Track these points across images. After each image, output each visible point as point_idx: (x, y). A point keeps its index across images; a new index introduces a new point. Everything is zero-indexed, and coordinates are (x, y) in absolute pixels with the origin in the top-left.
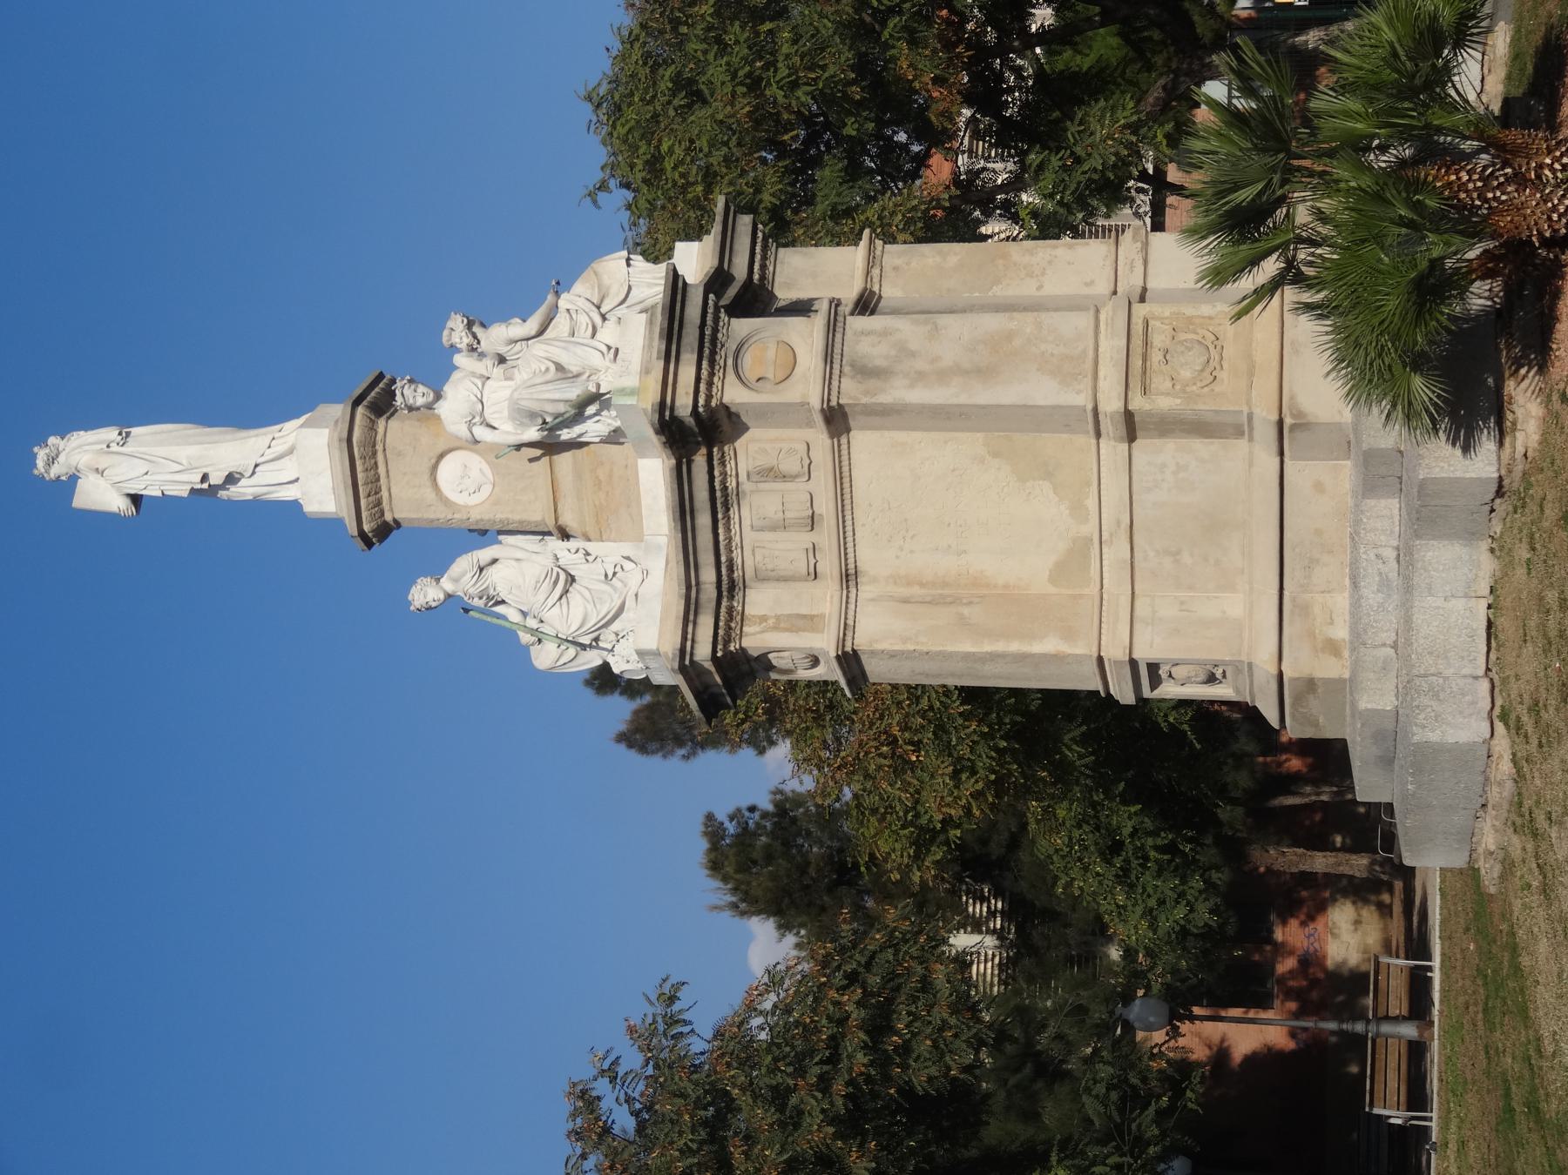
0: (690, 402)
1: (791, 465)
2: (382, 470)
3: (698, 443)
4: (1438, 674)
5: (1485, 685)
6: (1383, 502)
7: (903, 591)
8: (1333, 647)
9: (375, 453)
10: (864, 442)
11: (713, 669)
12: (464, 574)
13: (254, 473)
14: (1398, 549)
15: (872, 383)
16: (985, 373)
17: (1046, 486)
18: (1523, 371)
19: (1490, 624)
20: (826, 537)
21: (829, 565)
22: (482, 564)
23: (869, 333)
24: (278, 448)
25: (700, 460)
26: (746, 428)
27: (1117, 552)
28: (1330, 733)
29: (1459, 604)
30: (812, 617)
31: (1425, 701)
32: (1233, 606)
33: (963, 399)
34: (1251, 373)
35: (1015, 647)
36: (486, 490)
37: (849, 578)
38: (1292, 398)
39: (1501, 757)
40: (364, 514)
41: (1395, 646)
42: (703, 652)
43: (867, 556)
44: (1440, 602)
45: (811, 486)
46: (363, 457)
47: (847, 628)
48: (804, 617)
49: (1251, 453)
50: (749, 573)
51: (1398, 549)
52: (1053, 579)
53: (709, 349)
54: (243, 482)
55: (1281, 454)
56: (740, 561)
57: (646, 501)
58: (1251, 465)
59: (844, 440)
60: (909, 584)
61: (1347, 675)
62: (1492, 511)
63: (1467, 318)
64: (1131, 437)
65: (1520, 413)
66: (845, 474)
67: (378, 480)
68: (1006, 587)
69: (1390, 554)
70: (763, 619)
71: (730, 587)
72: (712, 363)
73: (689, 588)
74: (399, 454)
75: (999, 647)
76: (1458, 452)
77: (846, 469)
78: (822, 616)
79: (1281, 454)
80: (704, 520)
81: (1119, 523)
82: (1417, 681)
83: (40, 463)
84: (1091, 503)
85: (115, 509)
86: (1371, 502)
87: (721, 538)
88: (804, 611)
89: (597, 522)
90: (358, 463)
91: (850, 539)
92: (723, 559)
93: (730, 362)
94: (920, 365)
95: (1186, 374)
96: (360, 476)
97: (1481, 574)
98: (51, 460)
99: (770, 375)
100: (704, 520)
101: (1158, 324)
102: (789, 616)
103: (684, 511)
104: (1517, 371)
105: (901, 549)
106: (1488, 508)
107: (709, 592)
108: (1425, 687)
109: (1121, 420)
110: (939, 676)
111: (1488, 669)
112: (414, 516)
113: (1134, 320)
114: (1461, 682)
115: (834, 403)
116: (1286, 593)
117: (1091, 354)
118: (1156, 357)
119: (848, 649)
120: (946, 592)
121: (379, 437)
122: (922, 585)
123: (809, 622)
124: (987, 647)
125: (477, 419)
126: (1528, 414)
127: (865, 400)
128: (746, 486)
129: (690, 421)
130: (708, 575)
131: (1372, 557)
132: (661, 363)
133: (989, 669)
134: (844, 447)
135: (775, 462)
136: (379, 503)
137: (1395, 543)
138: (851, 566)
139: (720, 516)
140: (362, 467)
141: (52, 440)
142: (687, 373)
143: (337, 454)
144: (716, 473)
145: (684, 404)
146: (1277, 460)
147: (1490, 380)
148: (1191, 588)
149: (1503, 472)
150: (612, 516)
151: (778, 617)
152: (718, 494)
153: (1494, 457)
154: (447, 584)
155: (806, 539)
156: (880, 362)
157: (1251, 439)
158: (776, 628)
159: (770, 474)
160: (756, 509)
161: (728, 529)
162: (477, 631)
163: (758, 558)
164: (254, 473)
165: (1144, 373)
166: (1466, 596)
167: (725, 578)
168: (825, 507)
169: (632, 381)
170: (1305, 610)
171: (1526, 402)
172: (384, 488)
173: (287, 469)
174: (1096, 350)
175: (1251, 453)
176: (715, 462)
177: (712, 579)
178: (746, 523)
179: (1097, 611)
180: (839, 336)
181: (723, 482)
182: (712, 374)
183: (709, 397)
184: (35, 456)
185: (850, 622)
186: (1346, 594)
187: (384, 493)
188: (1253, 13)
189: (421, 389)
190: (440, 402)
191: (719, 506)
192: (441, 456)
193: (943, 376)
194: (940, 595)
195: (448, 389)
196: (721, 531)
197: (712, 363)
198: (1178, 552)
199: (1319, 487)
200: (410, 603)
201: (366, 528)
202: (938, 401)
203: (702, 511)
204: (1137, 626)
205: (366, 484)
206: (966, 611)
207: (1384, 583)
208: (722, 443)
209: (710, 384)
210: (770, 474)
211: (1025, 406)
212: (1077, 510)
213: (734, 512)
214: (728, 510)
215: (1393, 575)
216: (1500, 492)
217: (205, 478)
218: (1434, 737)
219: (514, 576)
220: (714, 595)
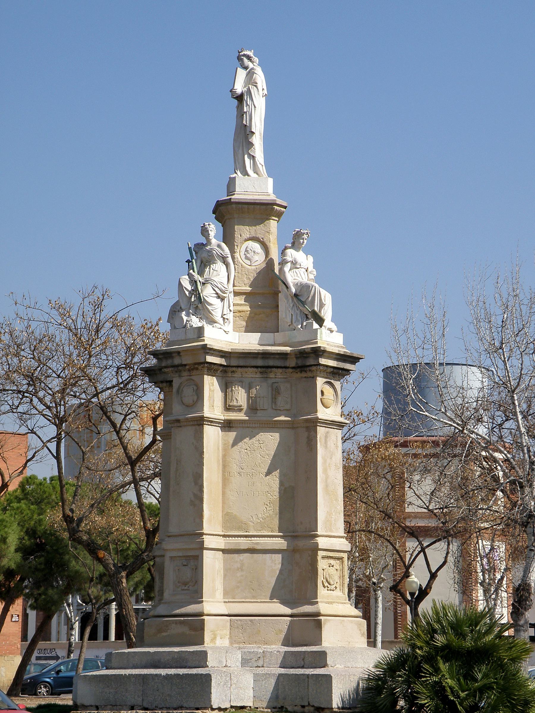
4: (231, 685)
8: (213, 640)
32: (219, 595)
41: (226, 666)
80: (260, 362)
94: (328, 461)
99: (324, 397)
106: (307, 704)
114: (229, 695)
118: (332, 562)
145: (323, 361)
156: (328, 446)
193: (325, 471)
198: (242, 570)
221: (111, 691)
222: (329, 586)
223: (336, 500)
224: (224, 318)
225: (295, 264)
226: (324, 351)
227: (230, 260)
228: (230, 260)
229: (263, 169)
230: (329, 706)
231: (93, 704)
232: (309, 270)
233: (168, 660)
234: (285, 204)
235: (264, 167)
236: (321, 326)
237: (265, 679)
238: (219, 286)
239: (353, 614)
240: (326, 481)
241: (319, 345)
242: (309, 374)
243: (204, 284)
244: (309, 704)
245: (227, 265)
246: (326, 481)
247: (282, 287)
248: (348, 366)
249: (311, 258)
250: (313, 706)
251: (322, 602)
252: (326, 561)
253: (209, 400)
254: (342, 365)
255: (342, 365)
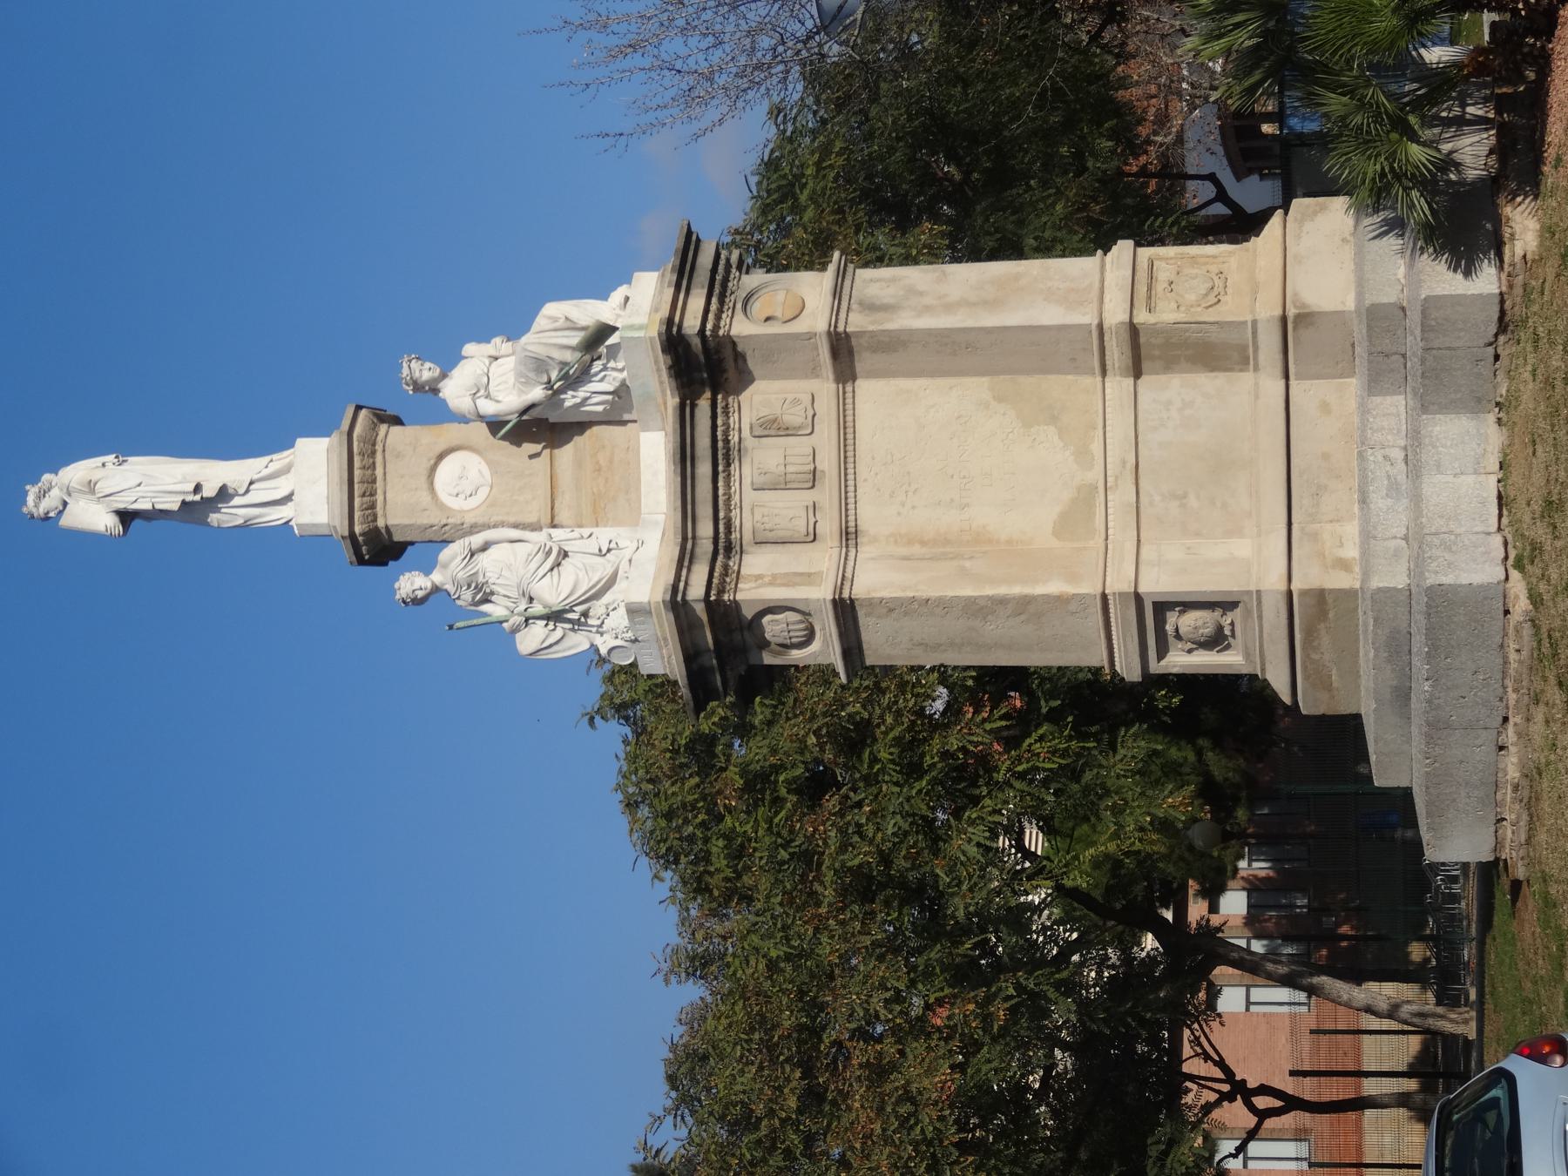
0: (698, 323)
1: (794, 417)
2: (379, 471)
3: (703, 383)
4: (1451, 532)
5: (1497, 541)
6: (1389, 399)
7: (904, 551)
8: (1343, 565)
9: (374, 453)
10: (869, 391)
11: (704, 618)
12: (454, 558)
13: (247, 491)
14: (1405, 448)
15: (879, 315)
16: (992, 304)
17: (1052, 428)
18: (1519, 199)
19: (1500, 497)
20: (826, 495)
21: (829, 526)
22: (474, 547)
23: (878, 280)
24: (273, 467)
25: (704, 404)
26: (752, 381)
27: (1122, 495)
28: (1345, 709)
29: (1470, 479)
30: (809, 575)
31: (1438, 553)
32: (1242, 548)
33: (970, 323)
34: (1255, 292)
35: (1017, 590)
36: (483, 493)
37: (849, 535)
38: (1296, 294)
39: (1517, 597)
40: (357, 515)
41: (1406, 538)
42: (696, 590)
43: (868, 515)
44: (1450, 478)
45: (813, 440)
46: (362, 454)
47: (843, 580)
48: (802, 574)
49: (1256, 384)
50: (747, 536)
51: (1405, 448)
52: (1057, 534)
53: (719, 289)
54: (237, 501)
55: (1287, 377)
56: (737, 523)
57: (645, 476)
58: (1257, 397)
59: (849, 388)
60: (910, 542)
61: (1357, 585)
62: (1497, 357)
63: (1462, 183)
64: (1137, 373)
65: (1518, 228)
66: (850, 424)
67: (374, 481)
68: (1009, 542)
69: (1398, 455)
70: (759, 577)
71: (726, 546)
72: (722, 302)
73: (685, 539)
74: (397, 456)
75: (1002, 590)
76: (1460, 276)
77: (849, 418)
78: (820, 574)
79: (1287, 377)
80: (704, 469)
81: (1124, 463)
82: (1429, 538)
83: (30, 499)
84: (1097, 447)
85: (101, 528)
86: (1378, 400)
87: (721, 492)
88: (801, 570)
89: (595, 511)
90: (357, 459)
91: (851, 494)
92: (722, 515)
93: (739, 306)
94: (927, 300)
95: (1191, 297)
96: (357, 473)
97: (1490, 449)
98: (43, 494)
99: (778, 314)
100: (704, 469)
101: (1163, 264)
102: (787, 574)
103: (684, 457)
104: (1513, 199)
105: (903, 505)
106: (1491, 350)
107: (705, 546)
108: (1436, 541)
109: (1126, 336)
110: (937, 647)
111: (1499, 529)
112: (406, 521)
113: (1139, 259)
114: (1474, 538)
115: (841, 329)
116: (1295, 527)
117: (1097, 285)
118: (1160, 287)
119: (846, 595)
120: (948, 549)
121: (380, 438)
122: (923, 543)
123: (808, 578)
124: (989, 591)
125: (482, 392)
126: (1526, 229)
127: (871, 328)
128: (749, 441)
129: (696, 343)
130: (705, 529)
131: (1380, 459)
132: (672, 290)
133: (993, 629)
134: (849, 395)
135: (779, 412)
136: (372, 506)
137: (1403, 443)
138: (852, 524)
139: (721, 468)
140: (359, 479)
141: (46, 477)
142: (696, 303)
143: (335, 458)
144: (719, 422)
145: (692, 324)
146: (1282, 382)
147: (1489, 226)
148: (1198, 534)
149: (1504, 289)
150: (609, 501)
151: (774, 576)
152: (720, 444)
153: (1495, 279)
154: (437, 577)
155: (807, 497)
156: (891, 301)
157: (1256, 369)
158: (771, 584)
159: (773, 428)
160: (760, 459)
161: (728, 486)
162: (458, 623)
163: (758, 517)
164: (247, 491)
165: (1149, 297)
166: (1476, 472)
167: (722, 535)
168: (828, 462)
169: (642, 319)
170: (1315, 537)
171: (1524, 226)
172: (379, 492)
173: (280, 489)
174: (1102, 281)
175: (1256, 384)
176: (719, 410)
177: (709, 529)
178: (747, 482)
179: (1102, 556)
180: (847, 283)
181: (726, 433)
182: (720, 311)
183: (716, 327)
184: (26, 493)
185: (849, 575)
186: (1356, 522)
187: (379, 498)
188: (1271, 873)
189: (428, 365)
190: (446, 381)
191: (720, 457)
192: (441, 457)
193: (949, 308)
194: (940, 547)
195: (456, 373)
196: (721, 484)
197: (722, 302)
198: (1185, 496)
199: (1325, 408)
200: (394, 592)
201: (358, 529)
202: (948, 325)
203: (703, 462)
204: (1142, 568)
205: (362, 482)
206: (968, 564)
207: (1393, 488)
208: (727, 395)
209: (718, 318)
210: (773, 428)
211: (1030, 327)
212: (1082, 455)
213: (734, 467)
214: (728, 465)
215: (1402, 478)
216: (1503, 326)
217: (198, 489)
218: (1448, 579)
219: (508, 567)
220: (710, 548)
221: (1463, 794)
222: (1216, 291)
223: (1017, 277)
224: (609, 550)
225: (482, 389)
226: (670, 321)
227: (477, 540)
228: (477, 540)
229: (279, 460)
230: (1497, 300)
231: (1493, 829)
232: (494, 353)
233: (1393, 670)
234: (350, 410)
235: (275, 457)
236: (614, 329)
237: (1434, 447)
238: (533, 565)
239: (1278, 232)
240: (974, 304)
241: (656, 334)
242: (728, 353)
243: (531, 599)
244: (1490, 344)
245: (485, 547)
246: (974, 304)
247: (534, 413)
248: (705, 259)
249: (469, 349)
250: (1496, 335)
251: (1253, 311)
252: (1161, 305)
253: (794, 585)
254: (702, 275)
255: (702, 275)
